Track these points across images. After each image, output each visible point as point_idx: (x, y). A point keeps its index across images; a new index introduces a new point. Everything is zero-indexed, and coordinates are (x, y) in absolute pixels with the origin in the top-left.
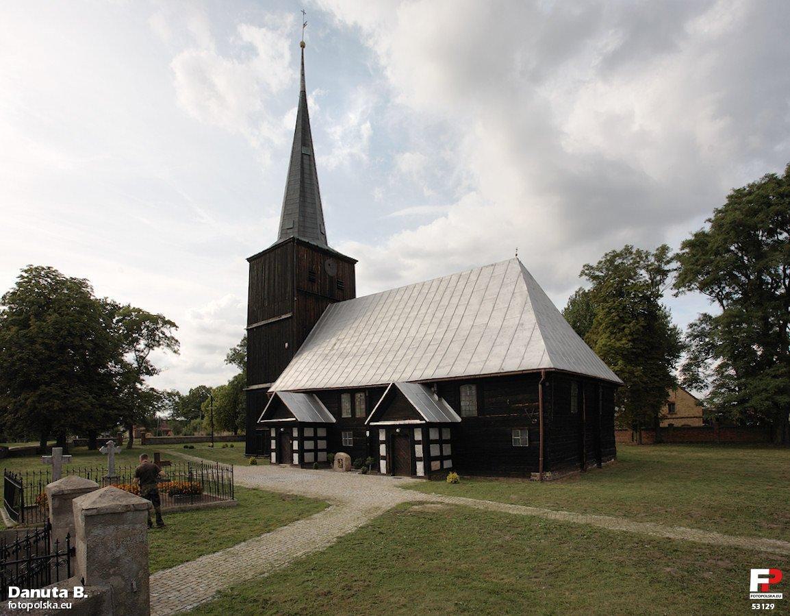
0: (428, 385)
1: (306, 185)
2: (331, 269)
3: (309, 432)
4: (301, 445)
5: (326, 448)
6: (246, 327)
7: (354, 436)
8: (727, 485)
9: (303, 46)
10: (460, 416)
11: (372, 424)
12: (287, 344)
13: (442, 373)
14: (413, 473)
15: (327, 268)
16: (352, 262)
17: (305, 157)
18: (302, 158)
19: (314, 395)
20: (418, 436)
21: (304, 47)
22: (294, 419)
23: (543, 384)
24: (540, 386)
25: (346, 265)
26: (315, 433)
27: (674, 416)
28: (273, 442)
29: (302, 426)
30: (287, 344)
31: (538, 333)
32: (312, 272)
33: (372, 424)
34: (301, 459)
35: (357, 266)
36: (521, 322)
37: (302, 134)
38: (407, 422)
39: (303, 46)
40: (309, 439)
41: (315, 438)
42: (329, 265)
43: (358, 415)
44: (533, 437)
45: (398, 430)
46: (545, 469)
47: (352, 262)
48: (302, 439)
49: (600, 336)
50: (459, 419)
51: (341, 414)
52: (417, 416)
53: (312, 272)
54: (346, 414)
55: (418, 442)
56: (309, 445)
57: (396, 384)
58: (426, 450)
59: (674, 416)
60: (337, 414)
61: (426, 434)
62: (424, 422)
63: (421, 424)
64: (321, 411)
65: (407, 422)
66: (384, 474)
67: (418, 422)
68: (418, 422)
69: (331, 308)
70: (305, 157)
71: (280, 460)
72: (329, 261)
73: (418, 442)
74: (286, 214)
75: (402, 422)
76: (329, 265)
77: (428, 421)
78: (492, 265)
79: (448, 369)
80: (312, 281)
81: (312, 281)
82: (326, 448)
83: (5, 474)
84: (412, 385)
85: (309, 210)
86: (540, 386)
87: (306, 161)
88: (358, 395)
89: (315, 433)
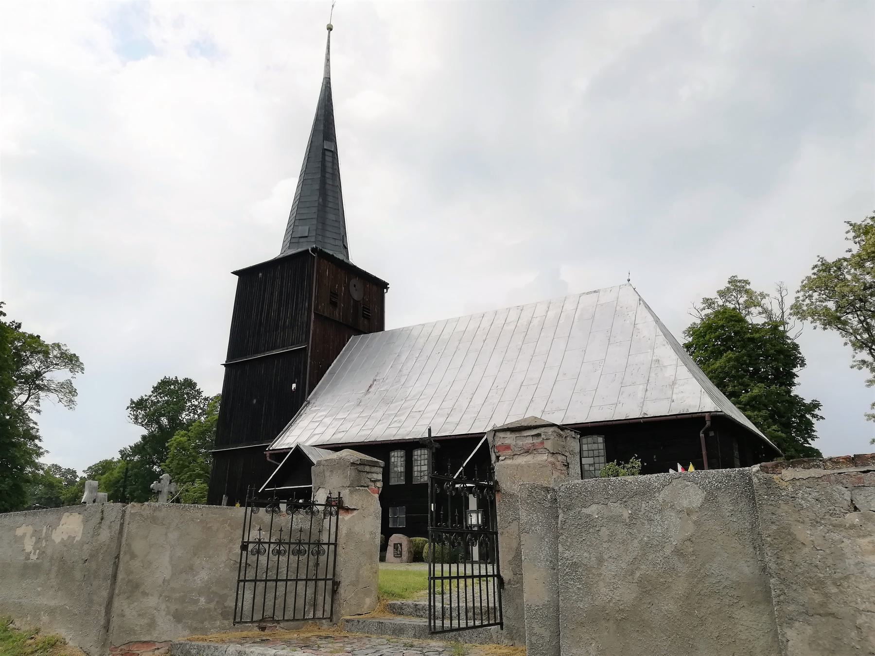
5: (280, 504)
7: (407, 513)
9: (330, 29)
12: (294, 386)
15: (352, 289)
16: (383, 285)
17: (327, 153)
18: (324, 155)
21: (331, 30)
23: (706, 434)
25: (375, 288)
30: (294, 386)
32: (334, 294)
36: (654, 358)
37: (325, 126)
39: (330, 29)
42: (355, 286)
47: (383, 285)
53: (334, 294)
69: (355, 341)
70: (327, 153)
72: (354, 281)
76: (355, 286)
80: (334, 304)
81: (334, 304)
82: (471, 579)
83: (331, 292)
85: (331, 216)
87: (329, 159)
88: (417, 453)
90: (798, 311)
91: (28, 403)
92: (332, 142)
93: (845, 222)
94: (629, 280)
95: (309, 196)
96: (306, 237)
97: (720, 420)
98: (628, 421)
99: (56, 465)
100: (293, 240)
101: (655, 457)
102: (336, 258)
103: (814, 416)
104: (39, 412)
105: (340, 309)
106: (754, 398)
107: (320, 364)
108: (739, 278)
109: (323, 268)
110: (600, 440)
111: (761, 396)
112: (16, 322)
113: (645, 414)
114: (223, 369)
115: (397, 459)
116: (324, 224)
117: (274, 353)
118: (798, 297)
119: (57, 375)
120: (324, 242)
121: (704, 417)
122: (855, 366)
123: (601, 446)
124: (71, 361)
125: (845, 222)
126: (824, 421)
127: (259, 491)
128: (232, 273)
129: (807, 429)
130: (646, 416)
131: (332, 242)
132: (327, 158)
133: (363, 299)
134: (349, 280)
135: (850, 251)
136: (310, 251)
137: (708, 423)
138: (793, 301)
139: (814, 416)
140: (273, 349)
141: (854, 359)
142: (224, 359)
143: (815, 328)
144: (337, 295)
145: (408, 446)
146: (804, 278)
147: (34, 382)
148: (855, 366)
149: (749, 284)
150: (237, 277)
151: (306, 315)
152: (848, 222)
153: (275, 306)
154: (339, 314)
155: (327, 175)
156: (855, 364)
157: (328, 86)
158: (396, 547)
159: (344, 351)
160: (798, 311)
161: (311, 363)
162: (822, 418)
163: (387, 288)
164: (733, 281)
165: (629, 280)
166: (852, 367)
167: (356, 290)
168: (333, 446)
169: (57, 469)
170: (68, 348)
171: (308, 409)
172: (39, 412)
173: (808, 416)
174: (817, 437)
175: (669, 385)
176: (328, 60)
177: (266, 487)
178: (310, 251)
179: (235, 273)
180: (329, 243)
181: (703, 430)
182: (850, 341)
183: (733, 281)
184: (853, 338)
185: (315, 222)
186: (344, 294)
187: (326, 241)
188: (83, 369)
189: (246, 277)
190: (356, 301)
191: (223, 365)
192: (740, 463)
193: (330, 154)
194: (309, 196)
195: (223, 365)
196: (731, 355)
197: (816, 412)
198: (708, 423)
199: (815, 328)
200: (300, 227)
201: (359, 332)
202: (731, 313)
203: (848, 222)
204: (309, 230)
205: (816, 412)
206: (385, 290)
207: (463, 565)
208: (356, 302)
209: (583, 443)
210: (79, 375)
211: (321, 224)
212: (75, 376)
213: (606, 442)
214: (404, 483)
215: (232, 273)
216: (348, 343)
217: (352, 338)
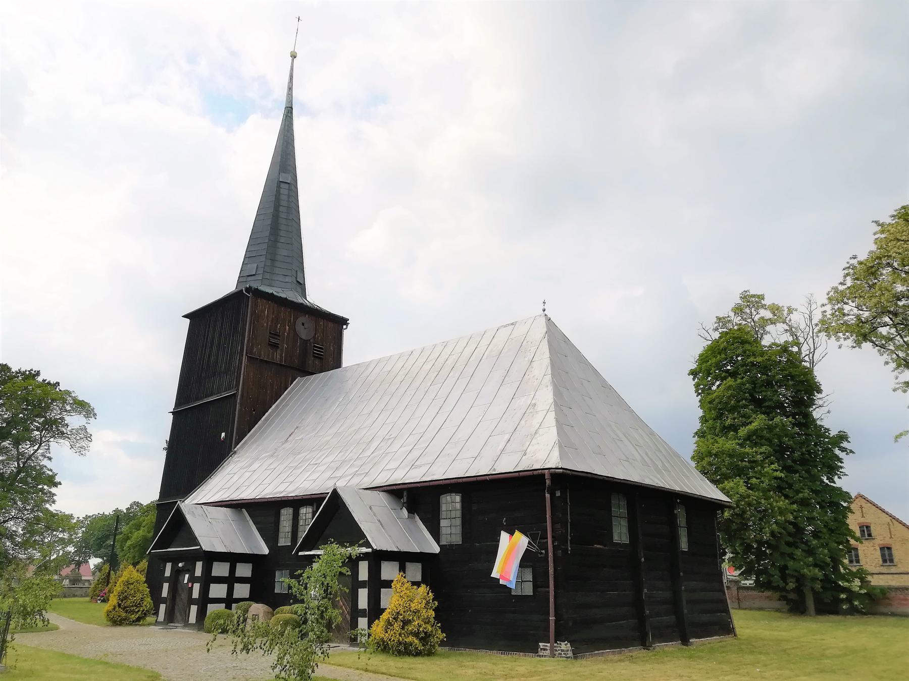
1: (281, 221)
2: (305, 329)
3: (220, 569)
4: (205, 590)
8: (132, 615)
9: (294, 56)
10: (438, 544)
11: (300, 553)
12: (223, 435)
13: (415, 476)
17: (282, 185)
18: (279, 187)
19: (244, 510)
21: (295, 57)
22: (198, 547)
24: (548, 496)
26: (232, 570)
27: (893, 570)
28: (166, 586)
29: (211, 557)
30: (223, 435)
31: (552, 415)
33: (300, 553)
34: (202, 614)
35: (348, 335)
39: (294, 56)
40: (219, 580)
41: (231, 580)
46: (559, 637)
50: (436, 549)
51: (277, 542)
54: (284, 541)
56: (218, 591)
57: (339, 490)
59: (893, 570)
62: (370, 550)
64: (248, 537)
67: (364, 550)
68: (364, 550)
71: (170, 618)
72: (302, 319)
74: (249, 257)
78: (512, 324)
79: (423, 470)
84: (376, 493)
85: (282, 252)
86: (548, 496)
87: (284, 191)
90: (826, 327)
91: (40, 451)
92: (289, 173)
93: (873, 222)
94: (544, 310)
95: (261, 232)
96: (254, 275)
99: (138, 503)
100: (241, 280)
102: (277, 296)
103: (843, 450)
104: (50, 459)
105: (282, 350)
106: (755, 432)
107: (254, 411)
108: (752, 293)
109: (261, 307)
110: (458, 498)
111: (761, 429)
112: (34, 370)
114: (171, 416)
116: (273, 260)
117: (211, 399)
118: (825, 312)
119: (74, 421)
120: (272, 280)
121: (544, 475)
122: (898, 389)
123: (458, 506)
124: (82, 407)
125: (873, 222)
126: (854, 455)
128: (183, 316)
129: (832, 467)
131: (281, 278)
132: (282, 191)
133: (314, 337)
134: (296, 319)
135: (855, 257)
137: (548, 482)
138: (820, 317)
139: (843, 450)
140: (211, 395)
141: (897, 381)
142: (171, 404)
143: (840, 347)
144: (279, 336)
145: (296, 503)
146: (830, 289)
147: (54, 428)
148: (898, 389)
149: (763, 299)
150: (188, 321)
151: (238, 358)
152: (876, 222)
154: (281, 356)
155: (281, 209)
156: (897, 386)
157: (289, 115)
159: (286, 395)
160: (826, 327)
161: (240, 410)
162: (851, 452)
163: (347, 324)
164: (746, 297)
165: (544, 310)
166: (894, 390)
167: (305, 328)
168: (229, 503)
169: (138, 506)
170: (76, 395)
171: (235, 458)
172: (50, 459)
173: (837, 451)
174: (845, 475)
175: (531, 434)
176: (290, 89)
177: (152, 549)
179: (185, 316)
180: (277, 280)
182: (892, 359)
183: (746, 297)
184: (894, 356)
185: (263, 259)
186: (288, 334)
187: (273, 279)
188: (95, 415)
189: (196, 318)
190: (304, 340)
191: (171, 412)
193: (286, 186)
194: (261, 232)
195: (171, 412)
196: (731, 383)
197: (845, 444)
199: (840, 347)
200: (249, 266)
201: (306, 372)
202: (734, 334)
203: (876, 222)
204: (257, 268)
205: (845, 444)
206: (345, 327)
208: (306, 341)
210: (92, 420)
211: (270, 261)
212: (89, 422)
213: (463, 501)
214: (290, 544)
215: (183, 316)
216: (292, 385)
217: (297, 380)
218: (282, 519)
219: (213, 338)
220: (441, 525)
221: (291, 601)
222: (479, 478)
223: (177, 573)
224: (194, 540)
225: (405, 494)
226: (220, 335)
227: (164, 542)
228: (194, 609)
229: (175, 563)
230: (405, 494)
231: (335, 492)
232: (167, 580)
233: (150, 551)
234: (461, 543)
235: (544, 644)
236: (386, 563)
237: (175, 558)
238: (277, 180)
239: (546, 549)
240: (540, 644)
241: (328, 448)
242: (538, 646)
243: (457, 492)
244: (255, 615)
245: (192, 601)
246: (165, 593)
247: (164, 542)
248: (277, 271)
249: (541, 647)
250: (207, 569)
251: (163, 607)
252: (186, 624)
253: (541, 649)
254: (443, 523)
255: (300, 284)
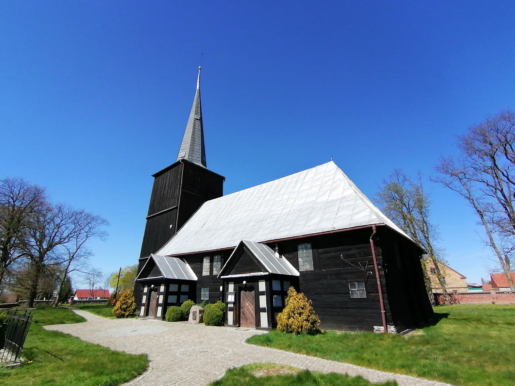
0: (272, 244)
4: (165, 299)
6: (146, 216)
10: (298, 271)
11: (222, 277)
12: (171, 226)
14: (258, 324)
20: (262, 286)
22: (163, 276)
26: (179, 288)
30: (171, 226)
33: (222, 277)
34: (164, 312)
37: (196, 109)
38: (252, 274)
40: (173, 293)
43: (215, 273)
44: (371, 288)
45: (244, 282)
48: (167, 294)
49: (190, 376)
50: (297, 274)
52: (261, 268)
54: (206, 273)
55: (262, 293)
57: (244, 242)
58: (270, 301)
60: (198, 271)
61: (269, 287)
62: (267, 273)
63: (265, 275)
65: (252, 274)
66: (230, 326)
68: (262, 274)
73: (262, 293)
75: (248, 275)
77: (271, 272)
89: (179, 288)
97: (383, 229)
98: (323, 233)
101: (341, 255)
113: (334, 228)
114: (146, 221)
115: (206, 263)
121: (372, 227)
127: (217, 277)
128: (152, 176)
130: (335, 229)
136: (181, 161)
137: (375, 231)
140: (165, 209)
153: (167, 188)
158: (194, 313)
163: (224, 180)
177: (138, 278)
178: (181, 161)
179: (153, 176)
181: (371, 237)
192: (382, 257)
198: (375, 231)
200: (182, 153)
207: (386, 289)
209: (299, 248)
215: (152, 176)
218: (204, 262)
219: (166, 183)
220: (299, 261)
221: (65, 303)
222: (325, 233)
223: (150, 291)
224: (160, 273)
225: (276, 245)
226: (165, 188)
227: (144, 274)
228: (160, 309)
229: (149, 286)
230: (276, 245)
231: (242, 244)
232: (145, 294)
233: (137, 279)
234: (313, 270)
235: (377, 327)
236: (274, 281)
237: (148, 283)
238: (194, 118)
239: (374, 271)
240: (374, 327)
241: (226, 228)
242: (373, 329)
243: (308, 243)
244: (194, 312)
245: (158, 305)
246: (144, 301)
247: (144, 274)
248: (194, 155)
249: (376, 329)
250: (167, 289)
251: (143, 308)
252: (156, 317)
253: (376, 330)
254: (300, 260)
255: (204, 162)
